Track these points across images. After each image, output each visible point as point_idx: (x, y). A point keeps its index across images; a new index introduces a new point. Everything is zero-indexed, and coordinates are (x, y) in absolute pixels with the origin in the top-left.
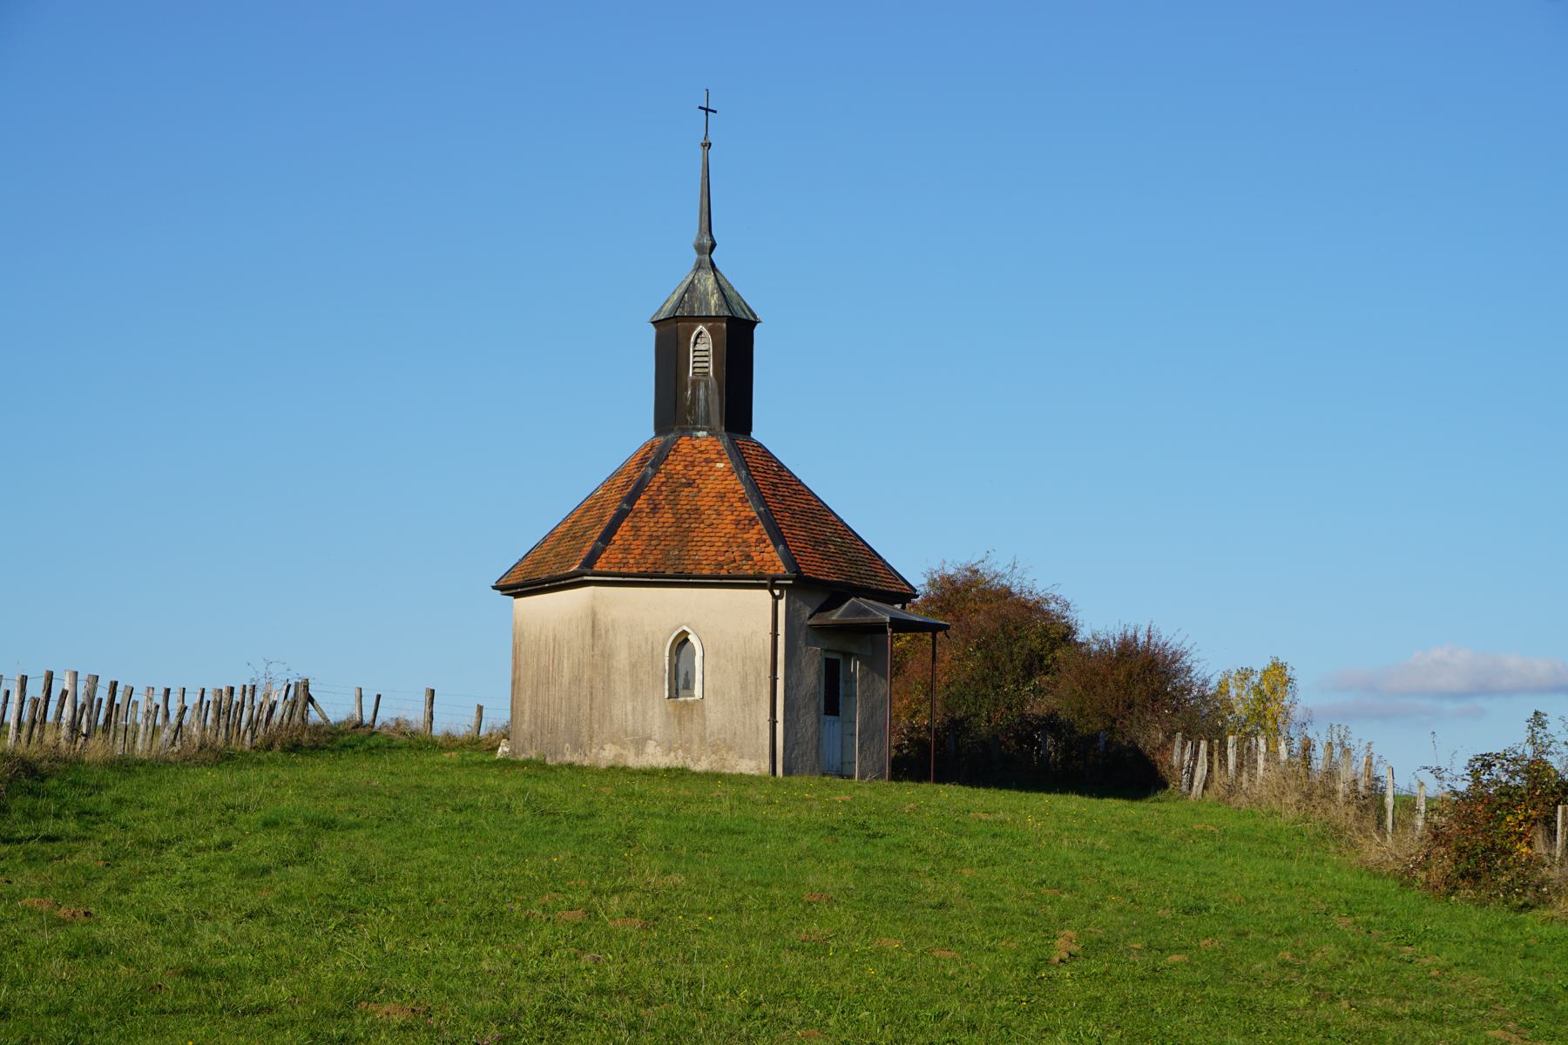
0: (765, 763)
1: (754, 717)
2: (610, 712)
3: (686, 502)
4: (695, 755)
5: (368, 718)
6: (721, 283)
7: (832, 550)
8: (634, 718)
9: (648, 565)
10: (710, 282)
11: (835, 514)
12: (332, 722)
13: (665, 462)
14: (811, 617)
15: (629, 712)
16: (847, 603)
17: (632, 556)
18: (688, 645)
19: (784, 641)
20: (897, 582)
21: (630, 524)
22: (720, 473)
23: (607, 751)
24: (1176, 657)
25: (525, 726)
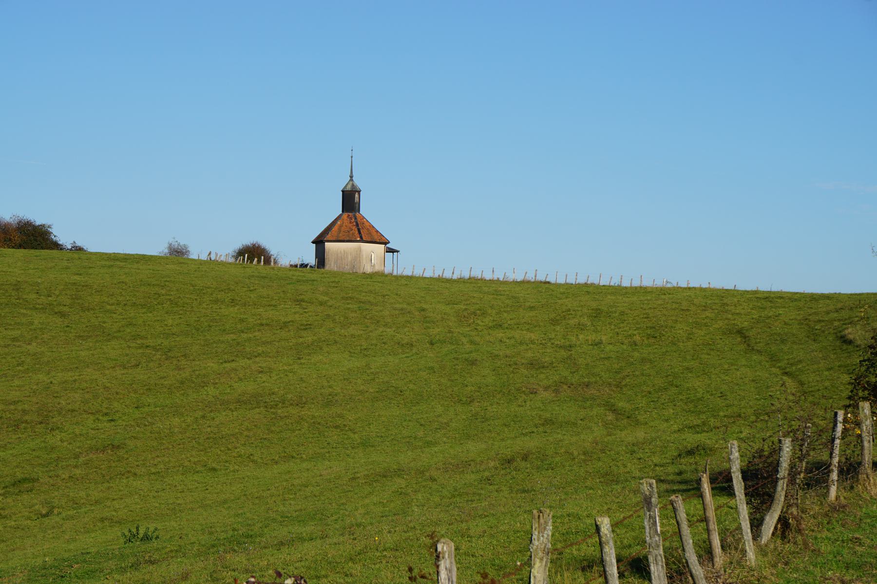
24: (254, 245)
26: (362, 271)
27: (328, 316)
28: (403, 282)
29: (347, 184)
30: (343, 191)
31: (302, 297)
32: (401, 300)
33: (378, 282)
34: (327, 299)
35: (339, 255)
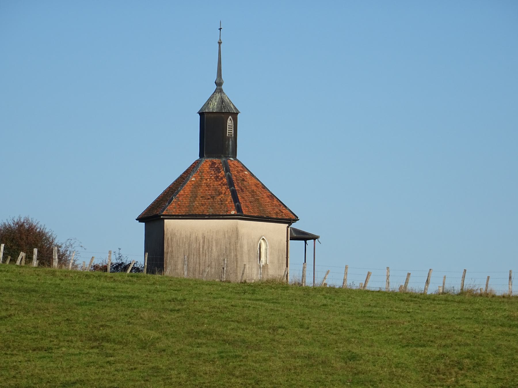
24: (21, 226)
26: (239, 279)
27: (156, 369)
28: (320, 300)
29: (210, 99)
30: (202, 114)
31: (104, 331)
32: (308, 338)
33: (267, 301)
34: (157, 335)
35: (194, 246)
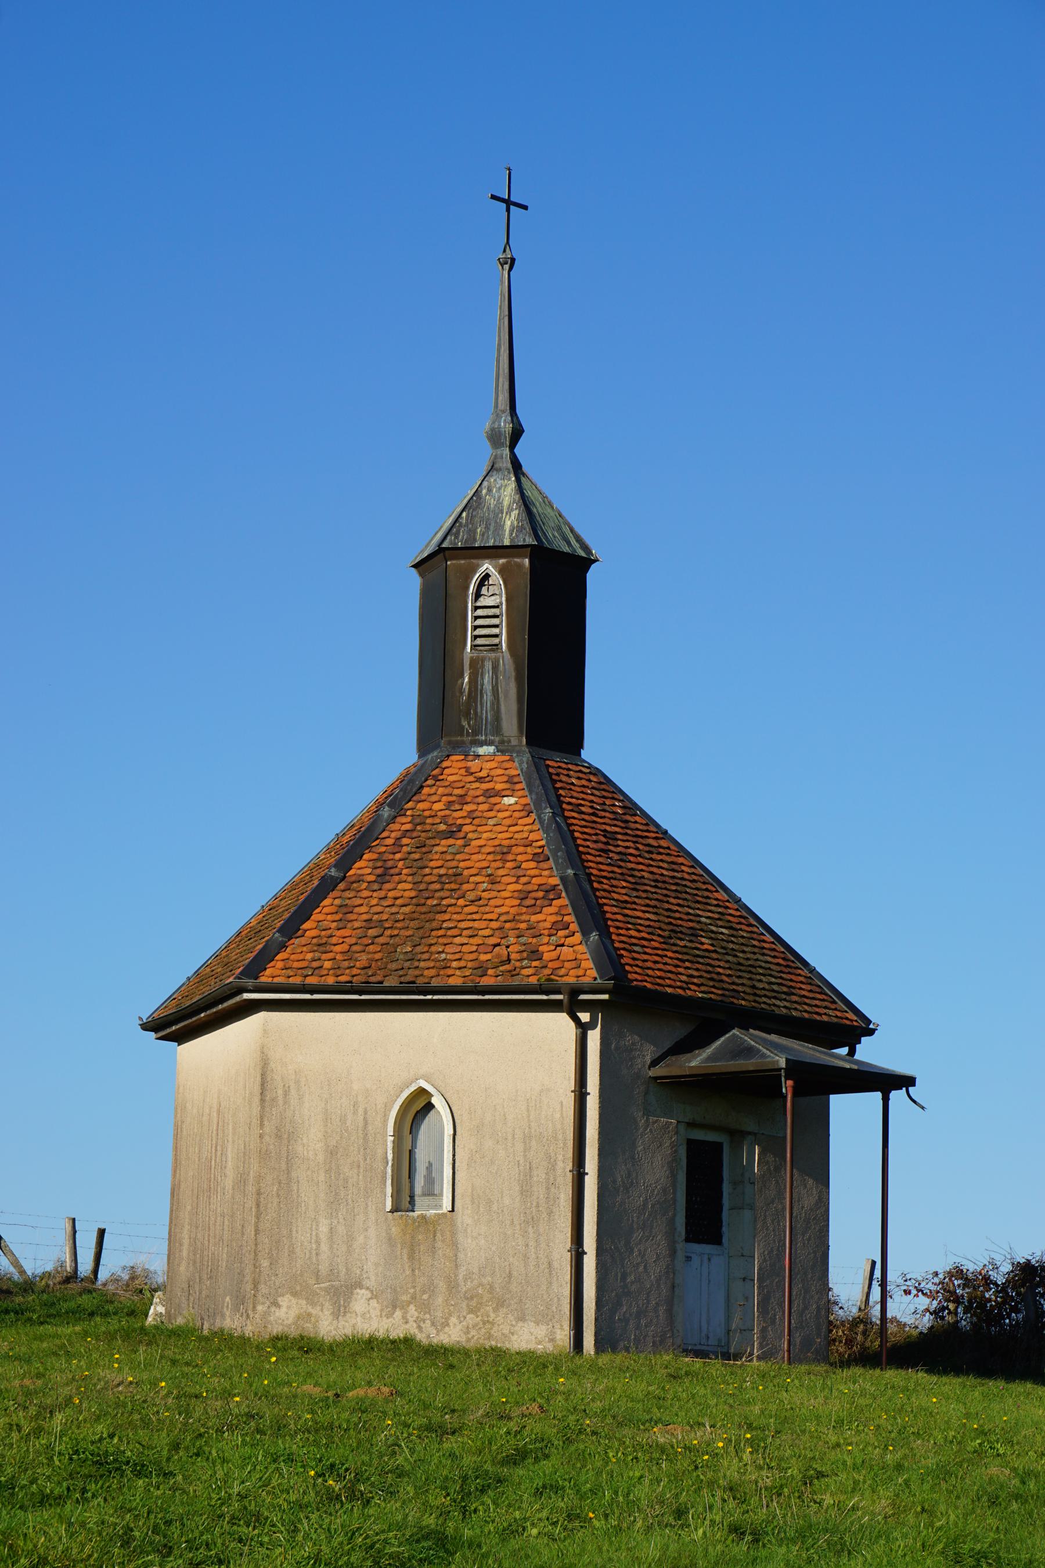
0: (562, 1328)
1: (543, 1245)
2: (290, 1236)
3: (439, 863)
4: (439, 1314)
5: (85, 1266)
6: (528, 493)
7: (705, 947)
8: (331, 1248)
9: (355, 971)
10: (506, 491)
11: (726, 889)
12: (29, 1273)
13: (415, 798)
14: (654, 1063)
15: (323, 1238)
16: (723, 1039)
17: (330, 955)
18: (432, 1112)
19: (597, 1106)
20: (833, 1006)
21: (337, 902)
22: (507, 814)
23: (284, 1310)
25: (182, 1268)
